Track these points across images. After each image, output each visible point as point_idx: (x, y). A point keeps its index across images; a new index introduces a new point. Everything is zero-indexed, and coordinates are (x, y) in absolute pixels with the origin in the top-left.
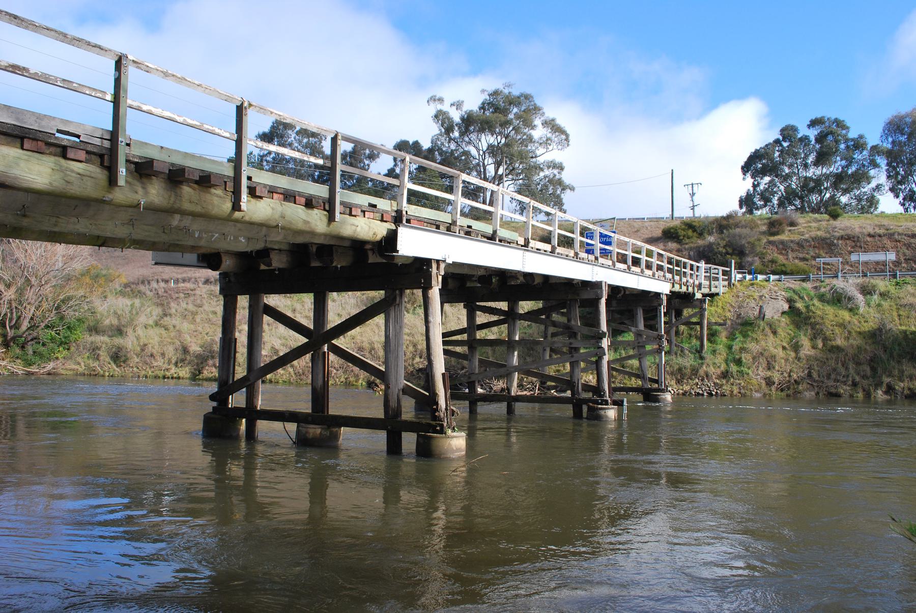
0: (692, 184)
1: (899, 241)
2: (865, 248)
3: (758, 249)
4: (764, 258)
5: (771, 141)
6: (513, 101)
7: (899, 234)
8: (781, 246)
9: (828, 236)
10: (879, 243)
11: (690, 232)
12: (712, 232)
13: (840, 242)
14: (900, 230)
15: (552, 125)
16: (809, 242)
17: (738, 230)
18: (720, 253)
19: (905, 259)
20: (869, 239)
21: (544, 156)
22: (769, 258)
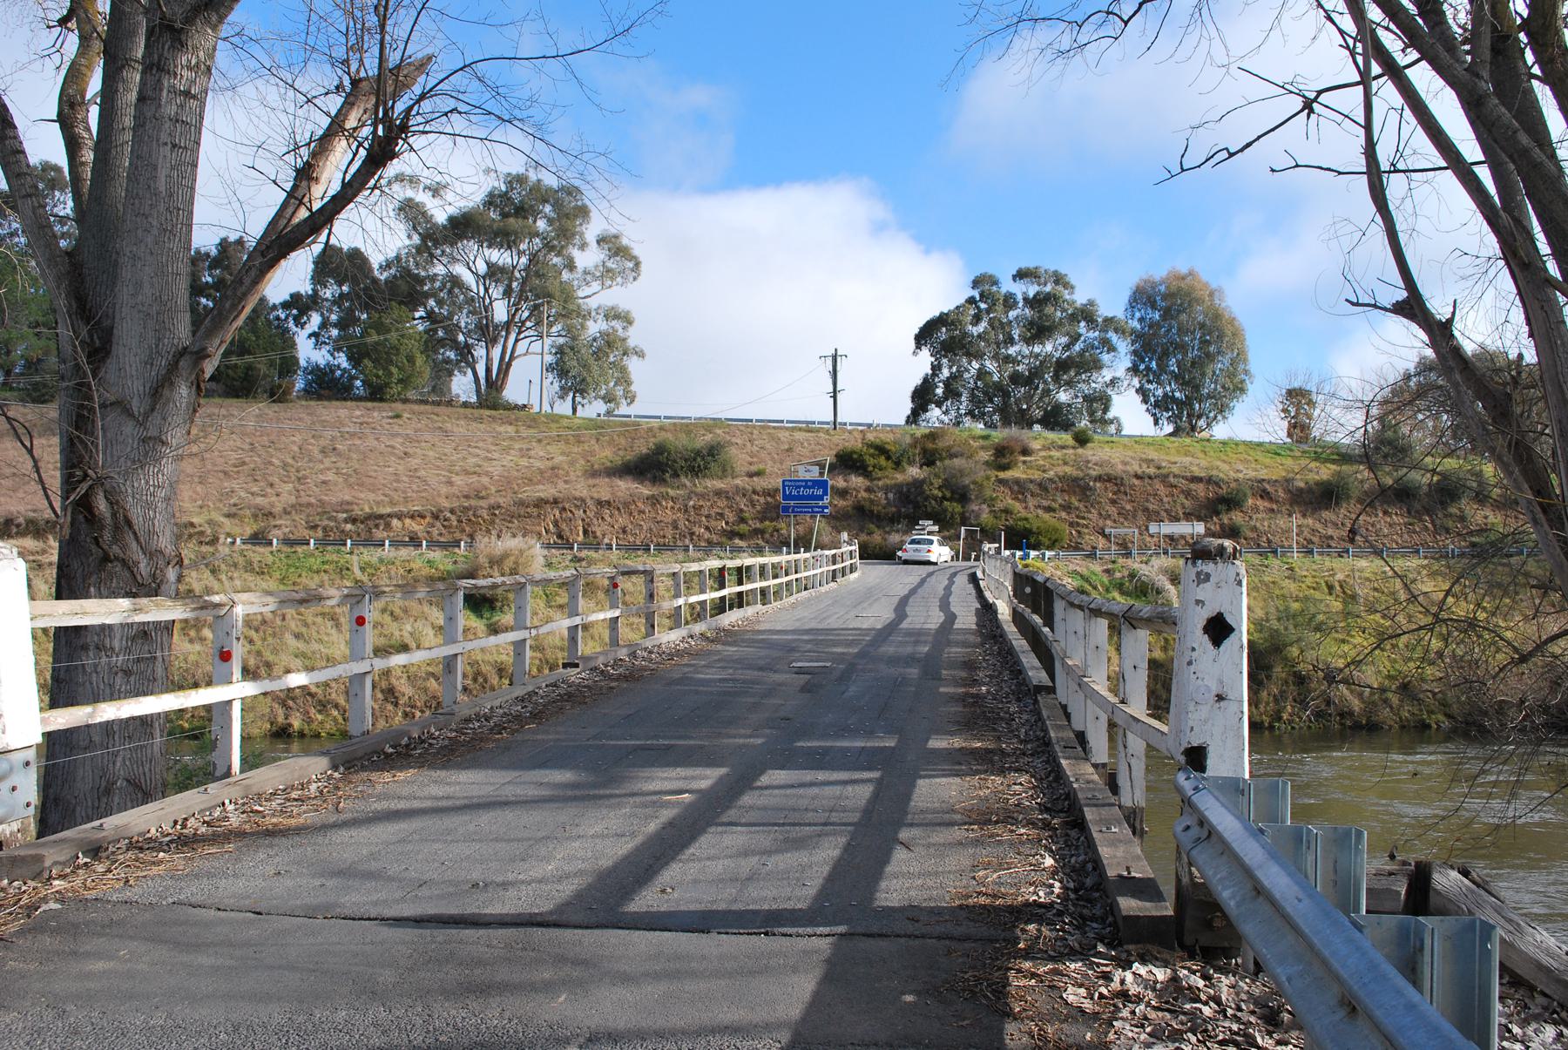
3: (988, 493)
5: (962, 301)
6: (542, 194)
7: (1175, 476)
8: (1016, 488)
9: (1081, 474)
11: (882, 461)
13: (1098, 485)
14: (1175, 470)
15: (613, 246)
17: (956, 462)
18: (935, 498)
20: (1136, 482)
21: (595, 297)
22: (999, 505)
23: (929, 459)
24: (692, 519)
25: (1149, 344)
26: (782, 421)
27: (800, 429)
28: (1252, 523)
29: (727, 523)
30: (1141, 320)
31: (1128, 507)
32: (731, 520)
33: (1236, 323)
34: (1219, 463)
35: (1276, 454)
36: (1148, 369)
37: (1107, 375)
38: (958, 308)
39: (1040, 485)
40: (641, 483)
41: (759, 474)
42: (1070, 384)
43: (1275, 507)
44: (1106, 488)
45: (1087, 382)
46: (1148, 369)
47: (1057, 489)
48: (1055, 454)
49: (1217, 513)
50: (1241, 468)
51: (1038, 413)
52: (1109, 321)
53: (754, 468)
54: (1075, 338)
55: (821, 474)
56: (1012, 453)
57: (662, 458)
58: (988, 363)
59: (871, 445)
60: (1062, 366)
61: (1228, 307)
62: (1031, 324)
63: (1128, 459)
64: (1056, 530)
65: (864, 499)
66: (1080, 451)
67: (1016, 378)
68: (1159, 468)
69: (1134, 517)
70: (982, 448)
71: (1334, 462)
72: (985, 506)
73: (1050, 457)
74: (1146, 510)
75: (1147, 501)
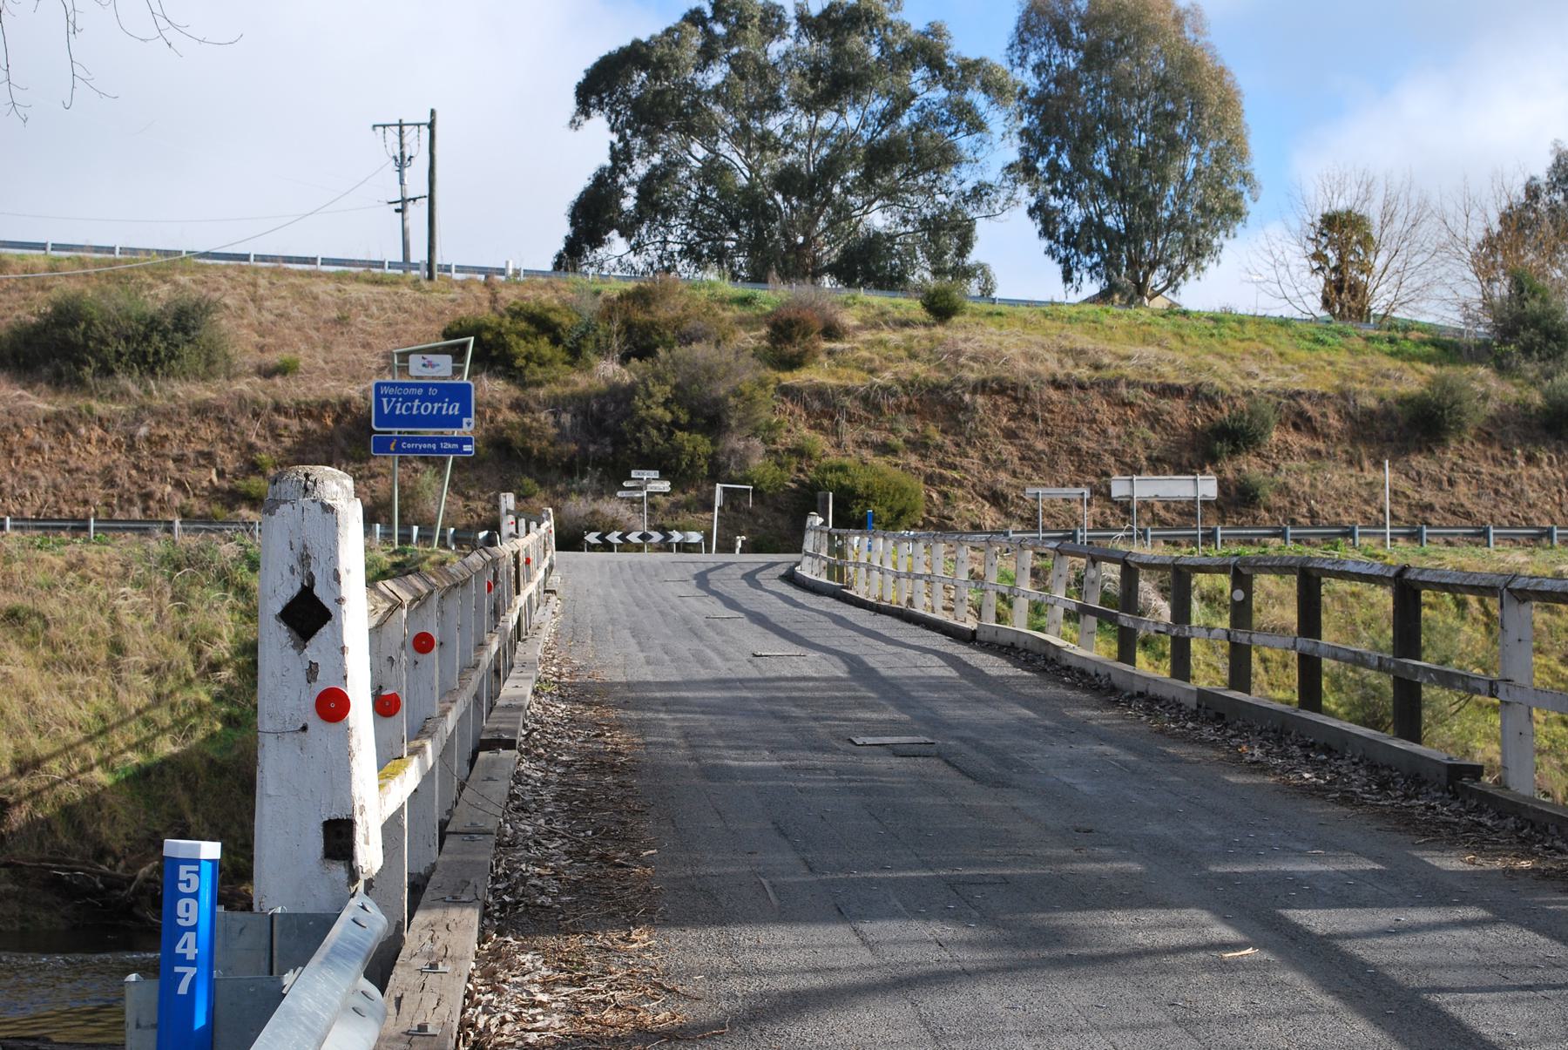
0: (401, 125)
1: (1131, 405)
2: (1045, 421)
3: (764, 414)
4: (774, 442)
5: (674, 19)
7: (1129, 384)
8: (817, 405)
9: (946, 379)
10: (1079, 406)
11: (544, 346)
12: (608, 346)
13: (980, 400)
14: (1129, 371)
16: (894, 395)
17: (699, 350)
18: (658, 425)
19: (1149, 459)
20: (1055, 395)
22: (785, 440)
23: (640, 344)
24: (144, 464)
25: (1058, 119)
26: (313, 261)
27: (356, 278)
28: (1280, 478)
29: (221, 474)
30: (1039, 68)
31: (1040, 445)
32: (229, 468)
33: (1227, 79)
34: (1210, 359)
35: (1317, 341)
36: (1054, 167)
37: (968, 177)
38: (669, 31)
39: (865, 399)
40: (29, 386)
41: (283, 370)
42: (891, 195)
43: (1320, 445)
44: (996, 407)
45: (929, 192)
46: (1054, 167)
47: (898, 407)
48: (893, 337)
49: (1213, 458)
50: (1254, 368)
51: (829, 253)
52: (971, 68)
53: (273, 358)
54: (904, 100)
55: (458, 371)
56: (805, 335)
57: (75, 334)
58: (724, 147)
59: (516, 314)
60: (880, 158)
61: (1208, 45)
62: (815, 70)
63: (1035, 349)
64: (902, 491)
65: (511, 425)
66: (939, 331)
67: (787, 180)
68: (1097, 367)
69: (1053, 464)
70: (741, 322)
71: (1428, 359)
72: (756, 442)
73: (881, 342)
74: (1074, 451)
75: (1077, 433)
